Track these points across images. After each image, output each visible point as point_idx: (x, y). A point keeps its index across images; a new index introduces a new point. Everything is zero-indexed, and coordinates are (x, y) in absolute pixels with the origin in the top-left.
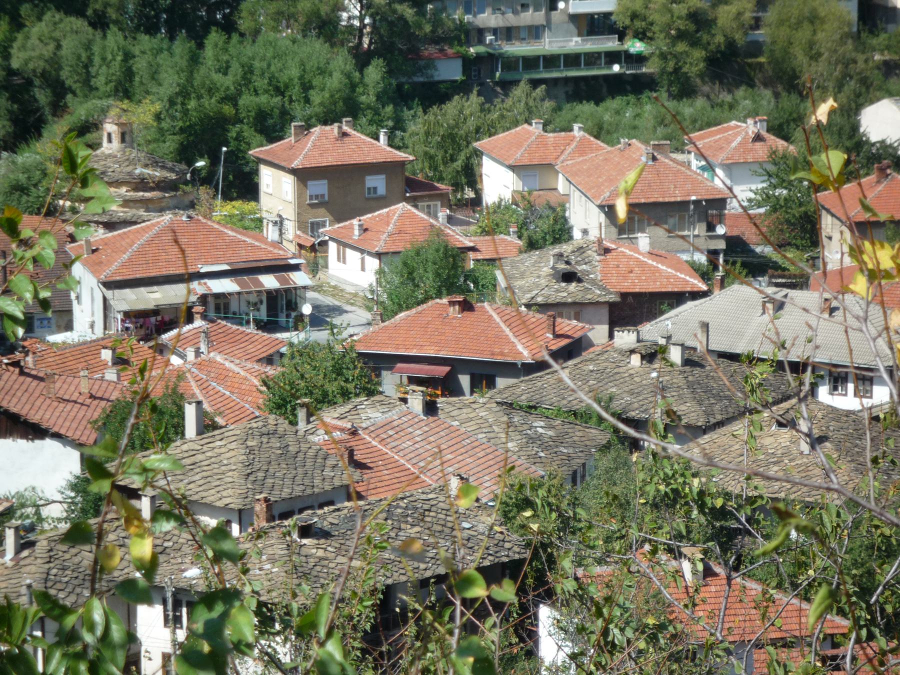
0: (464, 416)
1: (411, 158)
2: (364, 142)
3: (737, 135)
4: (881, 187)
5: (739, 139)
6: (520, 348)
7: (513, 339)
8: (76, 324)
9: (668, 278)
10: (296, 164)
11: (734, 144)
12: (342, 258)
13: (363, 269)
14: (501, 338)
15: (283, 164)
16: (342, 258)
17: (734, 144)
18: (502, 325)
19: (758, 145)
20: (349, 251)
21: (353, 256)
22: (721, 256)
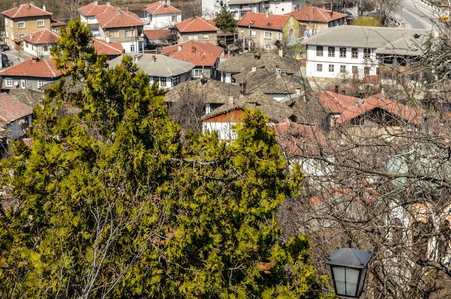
0: (18, 94)
1: (52, 14)
2: (37, 9)
3: (159, 5)
4: (193, 21)
5: (160, 7)
6: (53, 73)
7: (51, 70)
8: (352, 67)
9: (112, 50)
10: (86, 15)
11: (158, 8)
12: (27, 46)
13: (33, 49)
14: (48, 70)
15: (10, 16)
16: (27, 46)
17: (158, 8)
18: (49, 66)
19: (165, 8)
20: (29, 45)
21: (30, 45)
22: (143, 43)
